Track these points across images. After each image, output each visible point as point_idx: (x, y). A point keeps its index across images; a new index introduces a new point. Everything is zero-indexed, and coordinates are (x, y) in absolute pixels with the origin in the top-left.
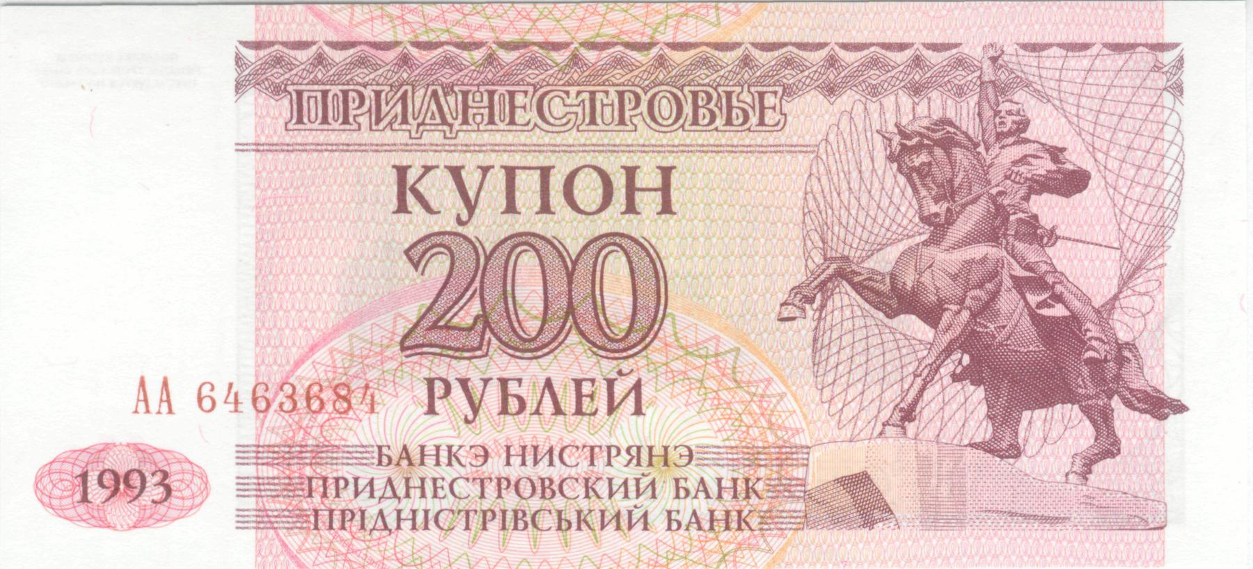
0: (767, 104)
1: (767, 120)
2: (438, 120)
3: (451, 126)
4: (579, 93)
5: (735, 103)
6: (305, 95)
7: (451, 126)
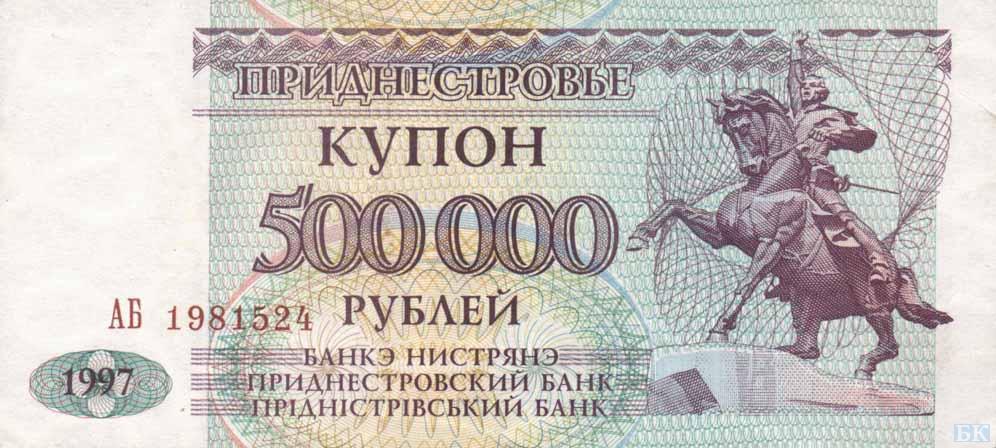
0: (620, 78)
1: (419, 91)
2: (356, 91)
3: (366, 95)
4: (469, 69)
5: (594, 77)
6: (249, 71)
7: (366, 95)
